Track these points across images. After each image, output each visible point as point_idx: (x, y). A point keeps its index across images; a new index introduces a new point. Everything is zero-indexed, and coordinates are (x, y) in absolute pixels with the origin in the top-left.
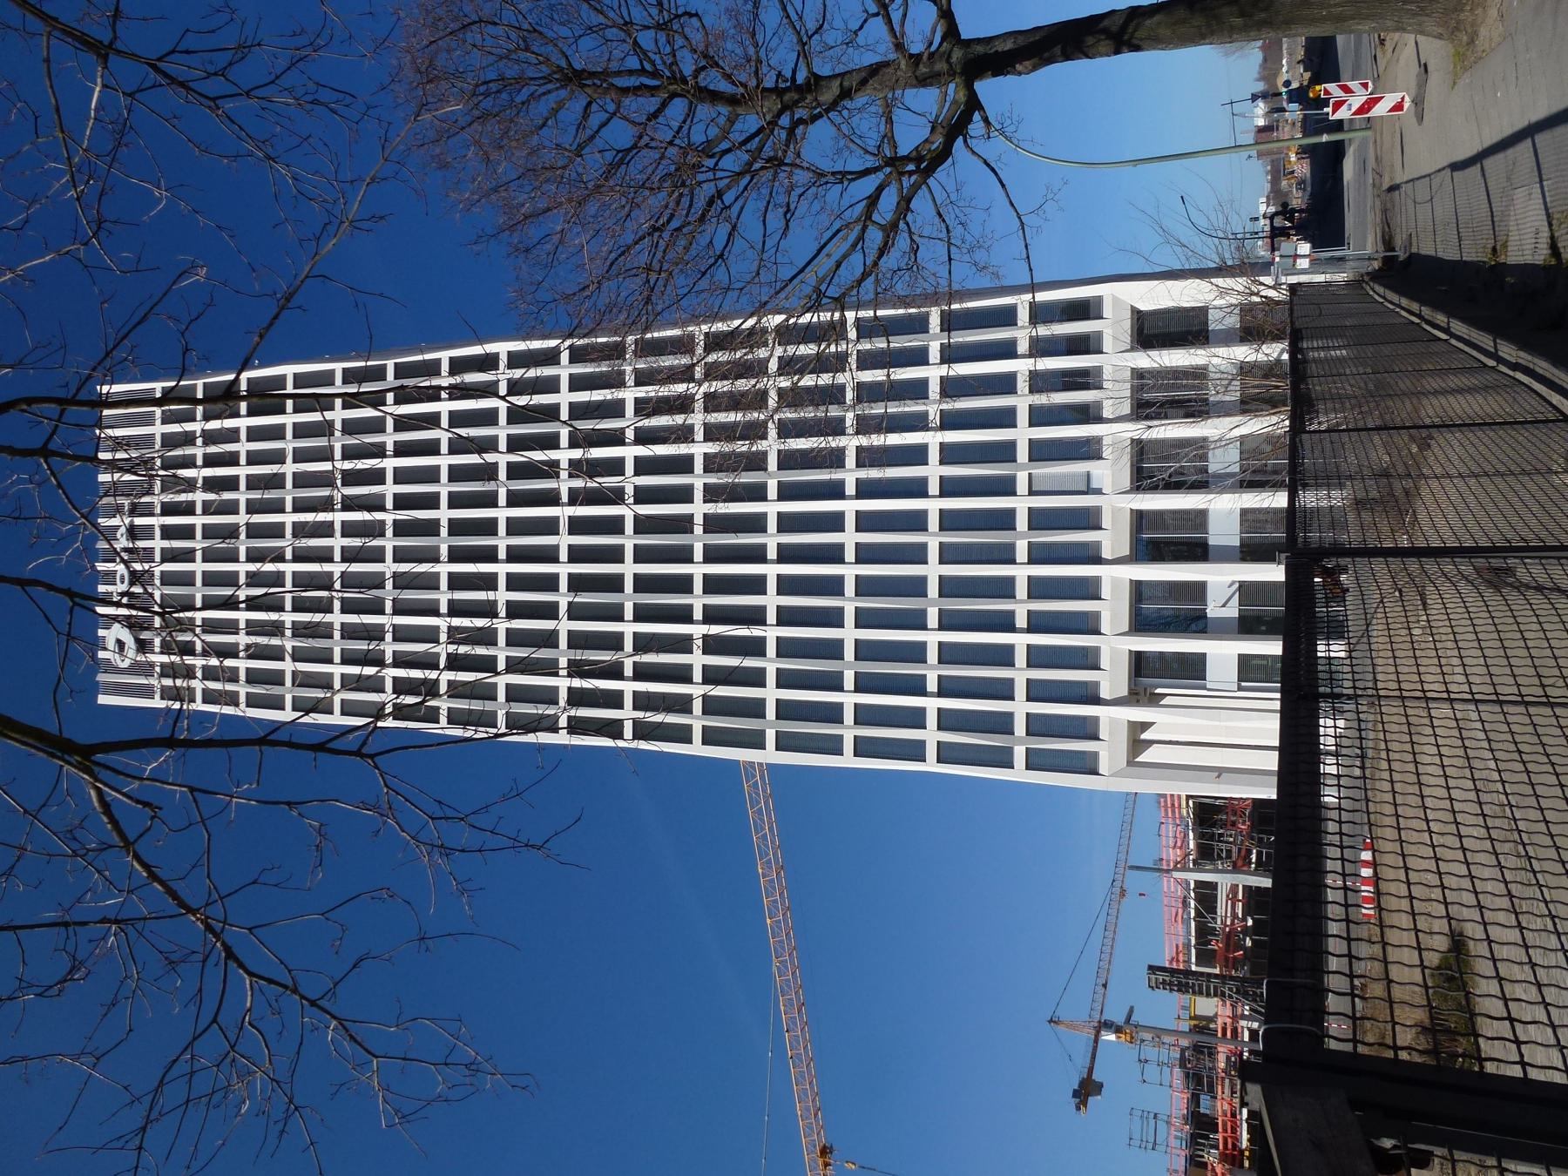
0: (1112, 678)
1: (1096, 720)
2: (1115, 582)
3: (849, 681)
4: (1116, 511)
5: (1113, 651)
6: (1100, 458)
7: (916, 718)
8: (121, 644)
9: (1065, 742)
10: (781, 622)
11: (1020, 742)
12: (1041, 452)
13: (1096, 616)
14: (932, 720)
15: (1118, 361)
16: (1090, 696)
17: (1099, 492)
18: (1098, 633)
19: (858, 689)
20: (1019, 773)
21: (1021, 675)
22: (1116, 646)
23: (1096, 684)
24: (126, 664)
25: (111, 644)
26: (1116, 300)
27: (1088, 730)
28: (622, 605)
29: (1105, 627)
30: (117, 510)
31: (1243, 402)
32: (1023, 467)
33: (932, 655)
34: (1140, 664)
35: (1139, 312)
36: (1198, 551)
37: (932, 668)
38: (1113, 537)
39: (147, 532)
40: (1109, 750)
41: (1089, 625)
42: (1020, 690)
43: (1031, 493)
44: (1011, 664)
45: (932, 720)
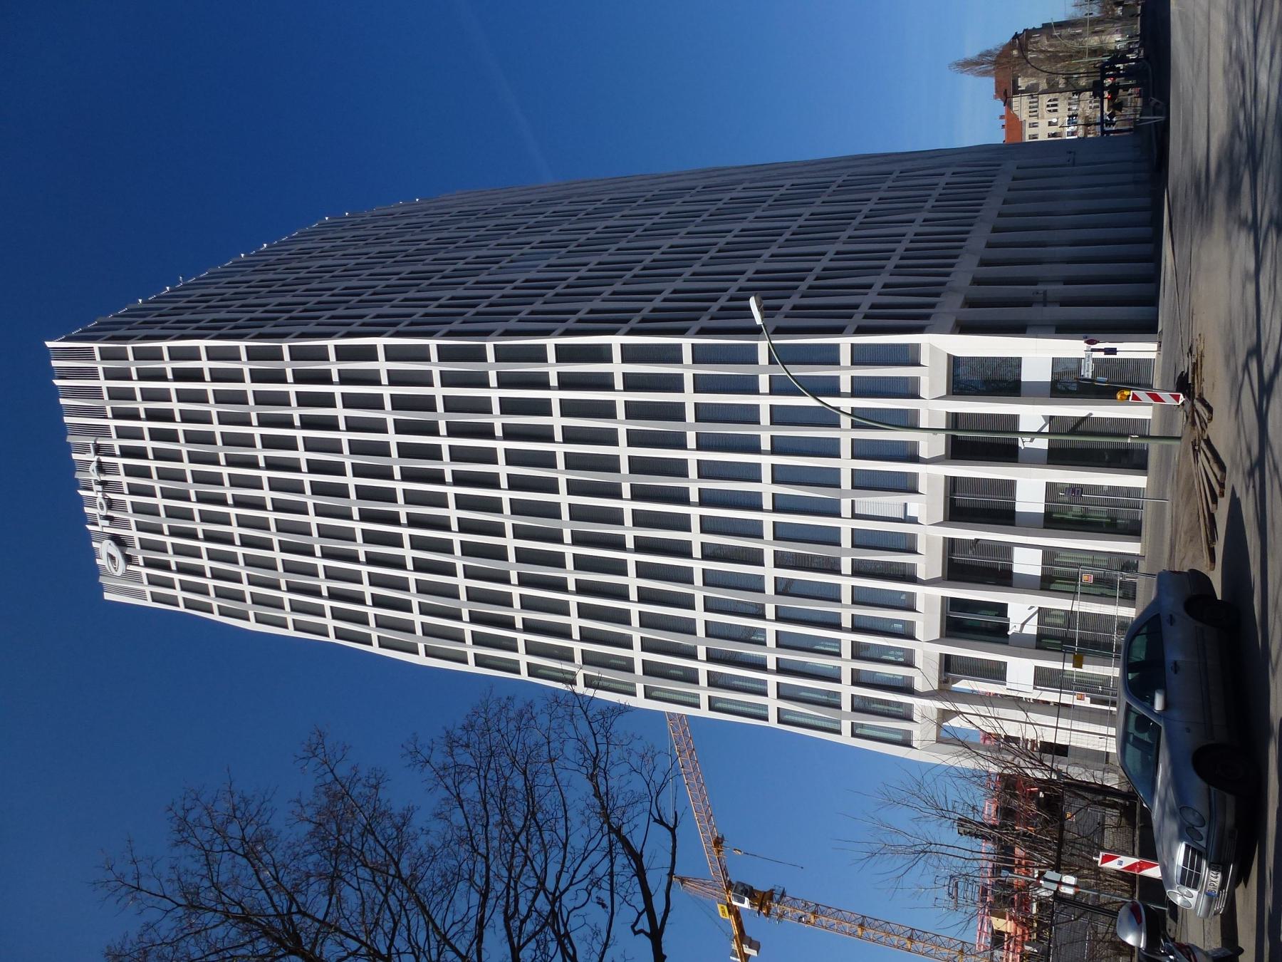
0: (925, 675)
1: (917, 347)
2: (930, 478)
3: (691, 441)
4: (929, 540)
5: (926, 656)
6: (916, 492)
7: (752, 473)
8: (112, 558)
9: (884, 701)
10: (628, 388)
11: (847, 553)
12: (863, 482)
13: (916, 381)
14: (766, 474)
15: (934, 407)
16: (908, 576)
17: (914, 521)
18: (918, 397)
19: (700, 447)
20: (846, 738)
21: (846, 435)
22: (928, 650)
23: (914, 566)
24: (119, 573)
25: (104, 556)
26: (933, 349)
27: (908, 421)
28: (487, 373)
29: (924, 392)
30: (84, 449)
31: (1040, 636)
32: (846, 494)
33: (765, 417)
34: (948, 665)
35: (955, 358)
36: (1008, 453)
37: (765, 429)
38: (928, 562)
39: (113, 469)
40: (922, 731)
41: (909, 390)
42: (846, 449)
43: (855, 516)
44: (836, 362)
45: (766, 474)
